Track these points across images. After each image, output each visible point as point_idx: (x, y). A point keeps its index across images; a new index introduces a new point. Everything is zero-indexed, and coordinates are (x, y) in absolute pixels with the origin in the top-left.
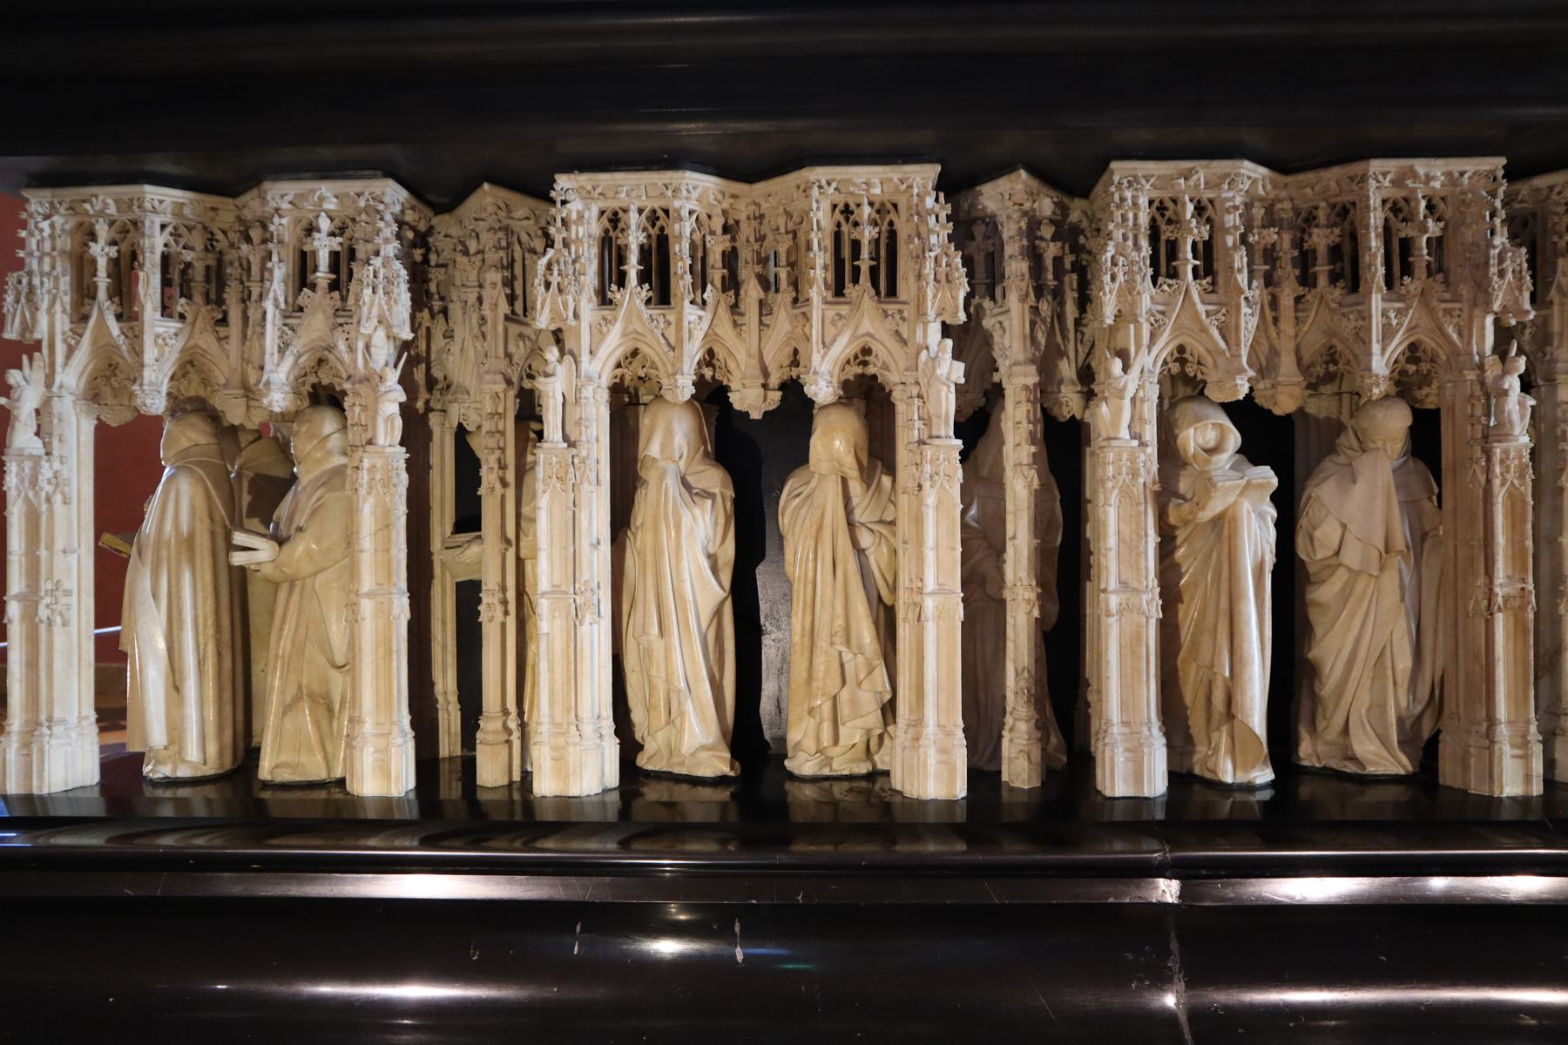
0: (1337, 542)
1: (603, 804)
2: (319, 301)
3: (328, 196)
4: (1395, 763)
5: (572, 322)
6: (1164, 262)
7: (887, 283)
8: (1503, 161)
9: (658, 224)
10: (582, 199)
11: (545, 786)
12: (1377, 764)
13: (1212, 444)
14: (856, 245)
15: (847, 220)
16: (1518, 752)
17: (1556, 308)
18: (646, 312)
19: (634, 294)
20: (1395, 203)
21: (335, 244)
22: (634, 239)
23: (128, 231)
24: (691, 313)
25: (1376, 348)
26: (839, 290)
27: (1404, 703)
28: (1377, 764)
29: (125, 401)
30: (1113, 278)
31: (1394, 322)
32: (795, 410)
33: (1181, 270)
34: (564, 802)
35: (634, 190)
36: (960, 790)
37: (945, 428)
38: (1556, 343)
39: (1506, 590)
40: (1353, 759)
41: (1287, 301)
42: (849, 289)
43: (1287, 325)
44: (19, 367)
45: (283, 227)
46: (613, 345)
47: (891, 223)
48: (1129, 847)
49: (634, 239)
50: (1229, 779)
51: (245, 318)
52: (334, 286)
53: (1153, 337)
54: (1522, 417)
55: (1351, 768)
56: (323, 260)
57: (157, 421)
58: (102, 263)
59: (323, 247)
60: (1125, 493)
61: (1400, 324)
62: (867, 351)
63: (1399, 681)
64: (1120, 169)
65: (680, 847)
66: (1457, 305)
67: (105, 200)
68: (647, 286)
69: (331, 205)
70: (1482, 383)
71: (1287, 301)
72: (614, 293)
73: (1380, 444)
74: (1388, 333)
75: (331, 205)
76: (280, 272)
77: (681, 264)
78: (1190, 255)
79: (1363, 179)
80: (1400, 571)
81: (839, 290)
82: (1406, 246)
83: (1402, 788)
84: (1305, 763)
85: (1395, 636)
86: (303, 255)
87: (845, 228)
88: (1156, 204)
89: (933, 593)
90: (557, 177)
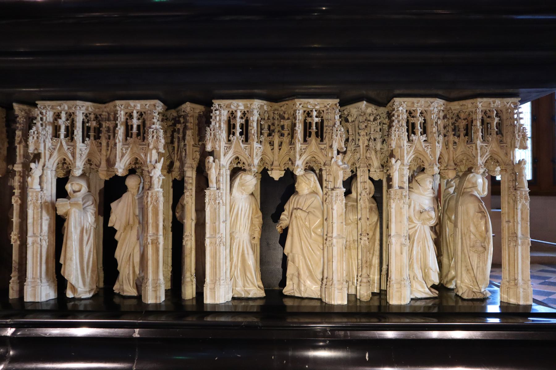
2: (313, 140)
3: (137, 105)
4: (133, 292)
5: (218, 149)
6: (411, 129)
7: (320, 134)
8: (338, 100)
9: (72, 117)
10: (402, 106)
11: (28, 298)
12: (128, 292)
13: (77, 190)
16: (154, 289)
18: (243, 146)
19: (237, 138)
20: (86, 114)
22: (239, 122)
23: (71, 116)
24: (256, 145)
25: (479, 158)
26: (305, 141)
27: (137, 272)
29: (385, 171)
30: (33, 138)
32: (290, 179)
33: (416, 133)
34: (214, 306)
35: (239, 106)
36: (345, 303)
37: (340, 183)
39: (152, 238)
41: (104, 143)
42: (308, 139)
43: (104, 152)
44: (35, 162)
45: (122, 116)
46: (231, 155)
47: (247, 118)
48: (367, 320)
49: (239, 122)
51: (108, 145)
52: (466, 134)
53: (51, 155)
54: (159, 182)
57: (124, 178)
58: (135, 127)
60: (35, 206)
61: (126, 152)
62: (237, 158)
64: (397, 100)
65: (332, 321)
67: (65, 106)
68: (467, 137)
69: (242, 108)
71: (104, 143)
72: (413, 137)
74: (408, 153)
75: (242, 108)
76: (121, 130)
77: (254, 128)
78: (419, 128)
79: (115, 106)
80: (138, 230)
82: (413, 125)
83: (136, 300)
85: (135, 251)
86: (56, 127)
87: (410, 118)
88: (408, 112)
89: (335, 238)
90: (213, 101)
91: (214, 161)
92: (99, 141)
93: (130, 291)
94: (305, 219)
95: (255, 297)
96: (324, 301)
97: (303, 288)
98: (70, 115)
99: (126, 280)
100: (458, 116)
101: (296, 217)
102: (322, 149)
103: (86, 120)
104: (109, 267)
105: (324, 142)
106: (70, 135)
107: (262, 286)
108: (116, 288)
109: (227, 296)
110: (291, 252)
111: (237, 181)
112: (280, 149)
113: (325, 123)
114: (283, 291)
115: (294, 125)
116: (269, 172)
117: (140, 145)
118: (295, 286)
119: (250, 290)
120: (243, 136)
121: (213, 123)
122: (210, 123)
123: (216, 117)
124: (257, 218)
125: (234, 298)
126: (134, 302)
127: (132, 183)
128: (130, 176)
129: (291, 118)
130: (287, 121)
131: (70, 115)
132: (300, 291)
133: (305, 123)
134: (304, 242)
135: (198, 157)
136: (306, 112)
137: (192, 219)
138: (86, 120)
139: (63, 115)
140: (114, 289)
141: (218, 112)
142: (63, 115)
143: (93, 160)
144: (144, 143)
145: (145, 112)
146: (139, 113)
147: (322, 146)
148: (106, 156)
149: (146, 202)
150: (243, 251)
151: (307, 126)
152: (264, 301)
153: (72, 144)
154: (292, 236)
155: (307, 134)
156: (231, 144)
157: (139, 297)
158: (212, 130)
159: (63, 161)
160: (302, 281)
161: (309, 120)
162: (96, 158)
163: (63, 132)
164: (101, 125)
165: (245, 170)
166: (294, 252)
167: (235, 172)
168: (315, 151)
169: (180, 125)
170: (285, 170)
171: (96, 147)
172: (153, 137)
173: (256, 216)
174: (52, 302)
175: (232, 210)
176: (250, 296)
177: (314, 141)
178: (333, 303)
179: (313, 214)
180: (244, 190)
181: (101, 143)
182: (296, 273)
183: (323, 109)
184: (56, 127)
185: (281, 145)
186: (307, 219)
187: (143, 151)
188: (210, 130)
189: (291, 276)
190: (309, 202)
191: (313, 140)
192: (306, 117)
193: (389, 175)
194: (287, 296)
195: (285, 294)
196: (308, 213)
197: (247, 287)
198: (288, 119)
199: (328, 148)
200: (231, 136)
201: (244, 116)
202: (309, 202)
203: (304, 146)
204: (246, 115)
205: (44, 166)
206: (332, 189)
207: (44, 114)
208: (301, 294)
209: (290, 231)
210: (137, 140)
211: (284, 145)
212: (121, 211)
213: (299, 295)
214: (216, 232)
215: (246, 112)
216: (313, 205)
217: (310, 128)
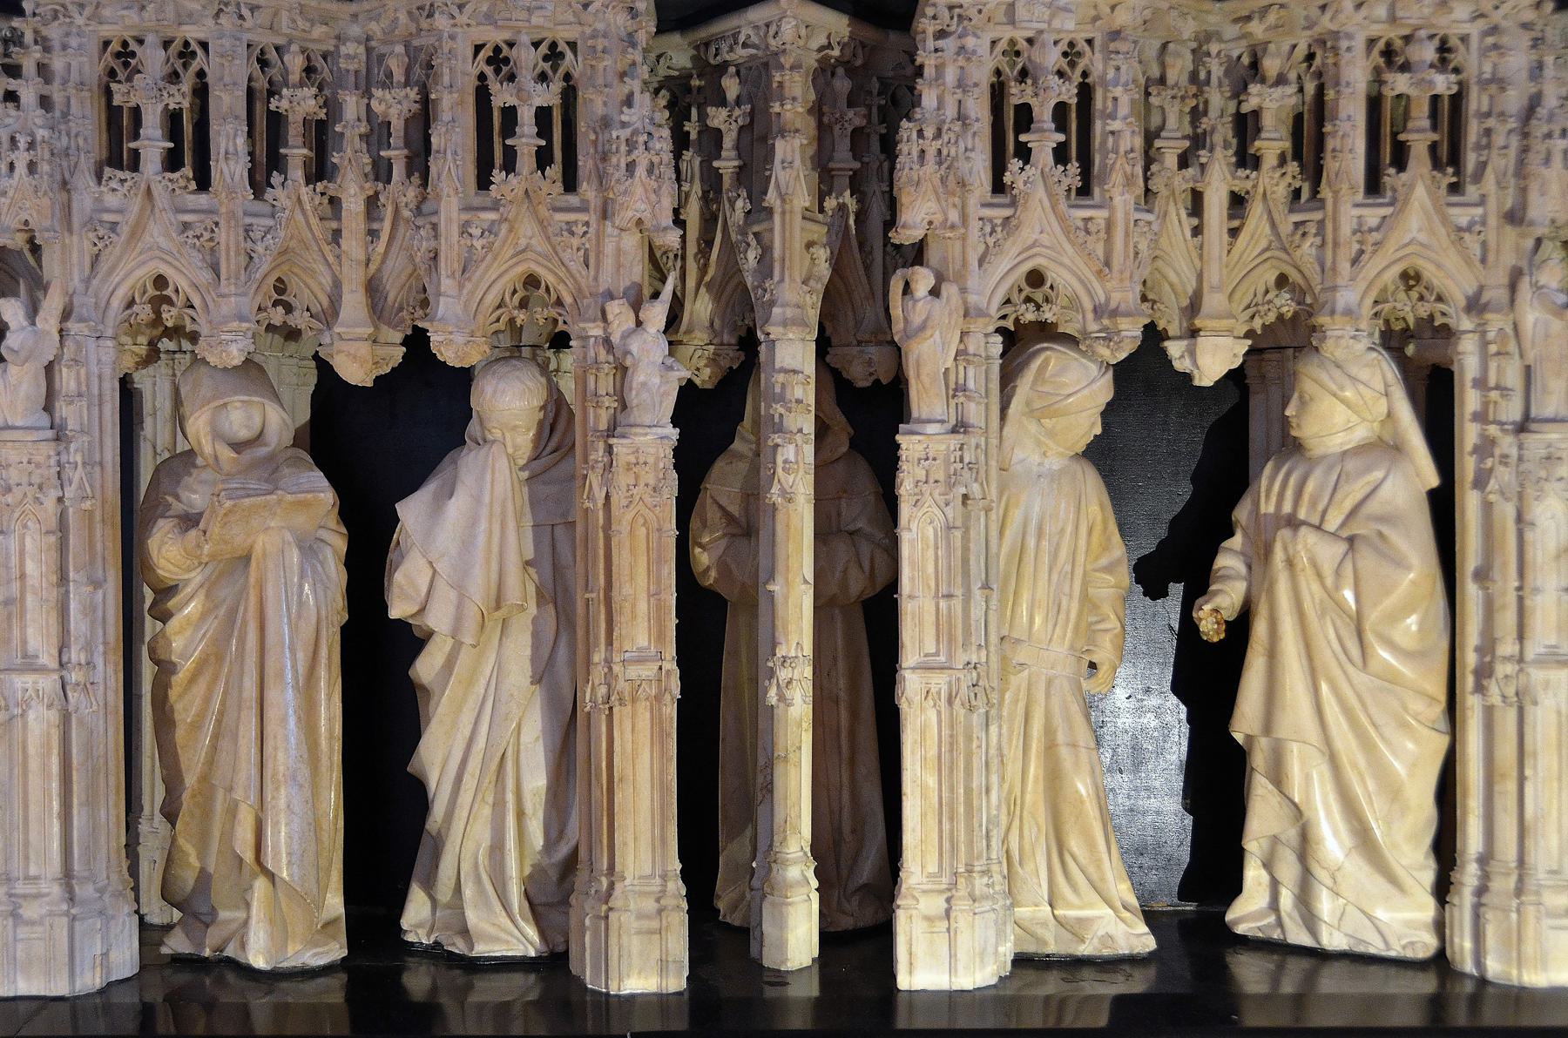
0: (424, 590)
1: (107, 1009)
2: (1418, 184)
4: (524, 941)
9: (195, 66)
14: (510, 114)
15: (497, 71)
17: (777, 218)
19: (1038, 180)
21: (549, 96)
26: (1374, 185)
28: (495, 939)
31: (478, 244)
38: (776, 277)
40: (465, 932)
41: (354, 204)
42: (1390, 177)
43: (353, 244)
47: (201, 74)
50: (259, 962)
55: (459, 947)
56: (526, 116)
59: (530, 96)
62: (1036, 278)
63: (529, 807)
66: (583, 217)
70: (607, 342)
71: (354, 204)
73: (497, 434)
77: (1118, 131)
81: (484, 183)
82: (1025, 117)
84: (410, 938)
85: (525, 738)
87: (494, 86)
91: (935, 292)
92: (332, 189)
93: (506, 933)
94: (1338, 573)
95: (1106, 952)
96: (1469, 967)
97: (1325, 905)
98: (186, 54)
99: (478, 880)
100: (125, 54)
101: (1290, 563)
102: (1460, 229)
103: (1010, 73)
104: (385, 824)
105: (1472, 192)
106: (188, 158)
107: (1134, 902)
108: (417, 918)
109: (1001, 949)
110: (1268, 728)
111: (1024, 386)
112: (1234, 233)
113: (1476, 101)
114: (1229, 917)
115: (424, 116)
116: (1174, 349)
117: (556, 209)
118: (1287, 900)
119: (1080, 920)
120: (1074, 167)
121: (929, 99)
122: (916, 102)
123: (940, 69)
124: (1108, 569)
125: (1022, 961)
126: (521, 987)
127: (508, 405)
128: (502, 369)
129: (1292, 76)
130: (1279, 91)
131: (186, 54)
132: (1310, 919)
133: (1374, 104)
134: (1335, 689)
135: (824, 270)
136: (1381, 45)
137: (806, 582)
138: (1010, 73)
139: (153, 60)
140: (405, 923)
141: (949, 44)
142: (153, 60)
143: (294, 284)
144: (573, 200)
145: (573, 45)
146: (544, 49)
147: (1462, 216)
148: (368, 261)
149: (600, 495)
150: (1049, 731)
151: (492, 127)
152: (1152, 972)
153: (203, 200)
154: (1273, 655)
155: (489, 162)
156: (1013, 204)
157: (553, 964)
158: (929, 132)
159: (151, 292)
160: (1321, 874)
161: (1400, 83)
162: (312, 273)
163: (152, 144)
164: (332, 107)
165: (1070, 340)
166: (1283, 730)
167: (1020, 341)
168: (1422, 237)
169: (724, 112)
170: (1249, 334)
171: (314, 221)
172: (631, 167)
173: (1104, 561)
174: (129, 998)
175: (1012, 535)
176: (1085, 950)
177: (1420, 193)
178: (1536, 978)
179: (1377, 550)
180: (1051, 434)
181: (334, 202)
182: (1291, 834)
183: (1466, 28)
184: (113, 114)
185: (1238, 202)
186: (1348, 569)
187: (575, 242)
188: (920, 133)
189: (1265, 844)
190: (1353, 493)
191: (1418, 184)
192: (1377, 71)
193: (751, 332)
194: (1245, 942)
195: (1240, 929)
196: (1351, 540)
197: (1070, 906)
198: (1281, 80)
199: (1493, 221)
200: (1014, 164)
201: (1072, 64)
202: (1353, 493)
203: (1372, 216)
204: (1082, 64)
205: (66, 315)
206: (1523, 426)
207: (56, 44)
208: (1314, 933)
209: (1260, 629)
210: (546, 186)
211: (1256, 210)
212: (460, 543)
213: (1305, 940)
214: (951, 639)
215: (1082, 46)
216: (1373, 507)
217: (136, 136)
